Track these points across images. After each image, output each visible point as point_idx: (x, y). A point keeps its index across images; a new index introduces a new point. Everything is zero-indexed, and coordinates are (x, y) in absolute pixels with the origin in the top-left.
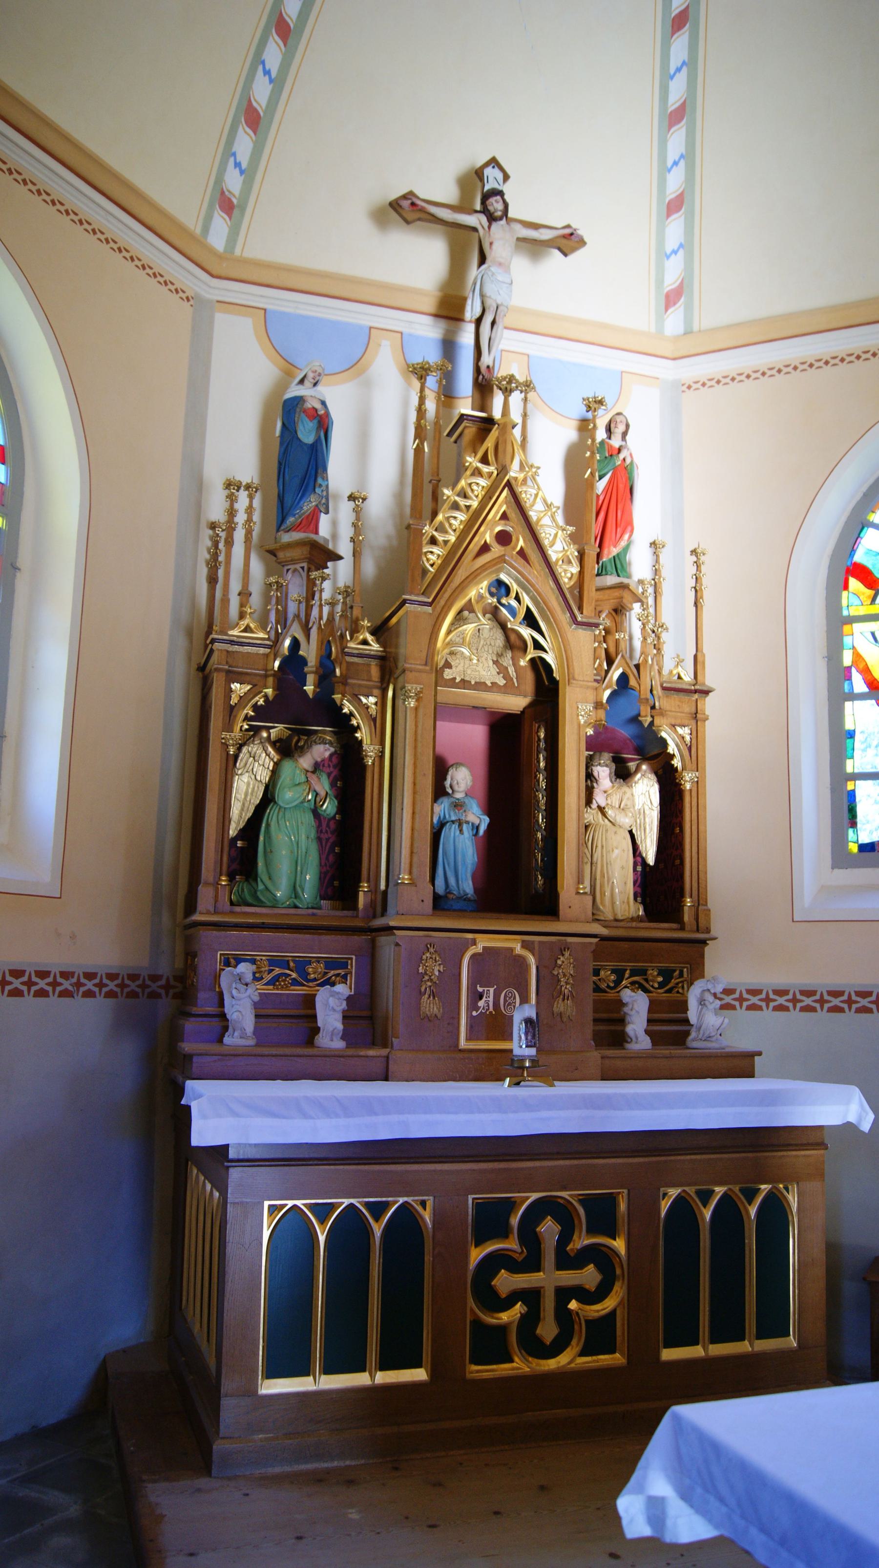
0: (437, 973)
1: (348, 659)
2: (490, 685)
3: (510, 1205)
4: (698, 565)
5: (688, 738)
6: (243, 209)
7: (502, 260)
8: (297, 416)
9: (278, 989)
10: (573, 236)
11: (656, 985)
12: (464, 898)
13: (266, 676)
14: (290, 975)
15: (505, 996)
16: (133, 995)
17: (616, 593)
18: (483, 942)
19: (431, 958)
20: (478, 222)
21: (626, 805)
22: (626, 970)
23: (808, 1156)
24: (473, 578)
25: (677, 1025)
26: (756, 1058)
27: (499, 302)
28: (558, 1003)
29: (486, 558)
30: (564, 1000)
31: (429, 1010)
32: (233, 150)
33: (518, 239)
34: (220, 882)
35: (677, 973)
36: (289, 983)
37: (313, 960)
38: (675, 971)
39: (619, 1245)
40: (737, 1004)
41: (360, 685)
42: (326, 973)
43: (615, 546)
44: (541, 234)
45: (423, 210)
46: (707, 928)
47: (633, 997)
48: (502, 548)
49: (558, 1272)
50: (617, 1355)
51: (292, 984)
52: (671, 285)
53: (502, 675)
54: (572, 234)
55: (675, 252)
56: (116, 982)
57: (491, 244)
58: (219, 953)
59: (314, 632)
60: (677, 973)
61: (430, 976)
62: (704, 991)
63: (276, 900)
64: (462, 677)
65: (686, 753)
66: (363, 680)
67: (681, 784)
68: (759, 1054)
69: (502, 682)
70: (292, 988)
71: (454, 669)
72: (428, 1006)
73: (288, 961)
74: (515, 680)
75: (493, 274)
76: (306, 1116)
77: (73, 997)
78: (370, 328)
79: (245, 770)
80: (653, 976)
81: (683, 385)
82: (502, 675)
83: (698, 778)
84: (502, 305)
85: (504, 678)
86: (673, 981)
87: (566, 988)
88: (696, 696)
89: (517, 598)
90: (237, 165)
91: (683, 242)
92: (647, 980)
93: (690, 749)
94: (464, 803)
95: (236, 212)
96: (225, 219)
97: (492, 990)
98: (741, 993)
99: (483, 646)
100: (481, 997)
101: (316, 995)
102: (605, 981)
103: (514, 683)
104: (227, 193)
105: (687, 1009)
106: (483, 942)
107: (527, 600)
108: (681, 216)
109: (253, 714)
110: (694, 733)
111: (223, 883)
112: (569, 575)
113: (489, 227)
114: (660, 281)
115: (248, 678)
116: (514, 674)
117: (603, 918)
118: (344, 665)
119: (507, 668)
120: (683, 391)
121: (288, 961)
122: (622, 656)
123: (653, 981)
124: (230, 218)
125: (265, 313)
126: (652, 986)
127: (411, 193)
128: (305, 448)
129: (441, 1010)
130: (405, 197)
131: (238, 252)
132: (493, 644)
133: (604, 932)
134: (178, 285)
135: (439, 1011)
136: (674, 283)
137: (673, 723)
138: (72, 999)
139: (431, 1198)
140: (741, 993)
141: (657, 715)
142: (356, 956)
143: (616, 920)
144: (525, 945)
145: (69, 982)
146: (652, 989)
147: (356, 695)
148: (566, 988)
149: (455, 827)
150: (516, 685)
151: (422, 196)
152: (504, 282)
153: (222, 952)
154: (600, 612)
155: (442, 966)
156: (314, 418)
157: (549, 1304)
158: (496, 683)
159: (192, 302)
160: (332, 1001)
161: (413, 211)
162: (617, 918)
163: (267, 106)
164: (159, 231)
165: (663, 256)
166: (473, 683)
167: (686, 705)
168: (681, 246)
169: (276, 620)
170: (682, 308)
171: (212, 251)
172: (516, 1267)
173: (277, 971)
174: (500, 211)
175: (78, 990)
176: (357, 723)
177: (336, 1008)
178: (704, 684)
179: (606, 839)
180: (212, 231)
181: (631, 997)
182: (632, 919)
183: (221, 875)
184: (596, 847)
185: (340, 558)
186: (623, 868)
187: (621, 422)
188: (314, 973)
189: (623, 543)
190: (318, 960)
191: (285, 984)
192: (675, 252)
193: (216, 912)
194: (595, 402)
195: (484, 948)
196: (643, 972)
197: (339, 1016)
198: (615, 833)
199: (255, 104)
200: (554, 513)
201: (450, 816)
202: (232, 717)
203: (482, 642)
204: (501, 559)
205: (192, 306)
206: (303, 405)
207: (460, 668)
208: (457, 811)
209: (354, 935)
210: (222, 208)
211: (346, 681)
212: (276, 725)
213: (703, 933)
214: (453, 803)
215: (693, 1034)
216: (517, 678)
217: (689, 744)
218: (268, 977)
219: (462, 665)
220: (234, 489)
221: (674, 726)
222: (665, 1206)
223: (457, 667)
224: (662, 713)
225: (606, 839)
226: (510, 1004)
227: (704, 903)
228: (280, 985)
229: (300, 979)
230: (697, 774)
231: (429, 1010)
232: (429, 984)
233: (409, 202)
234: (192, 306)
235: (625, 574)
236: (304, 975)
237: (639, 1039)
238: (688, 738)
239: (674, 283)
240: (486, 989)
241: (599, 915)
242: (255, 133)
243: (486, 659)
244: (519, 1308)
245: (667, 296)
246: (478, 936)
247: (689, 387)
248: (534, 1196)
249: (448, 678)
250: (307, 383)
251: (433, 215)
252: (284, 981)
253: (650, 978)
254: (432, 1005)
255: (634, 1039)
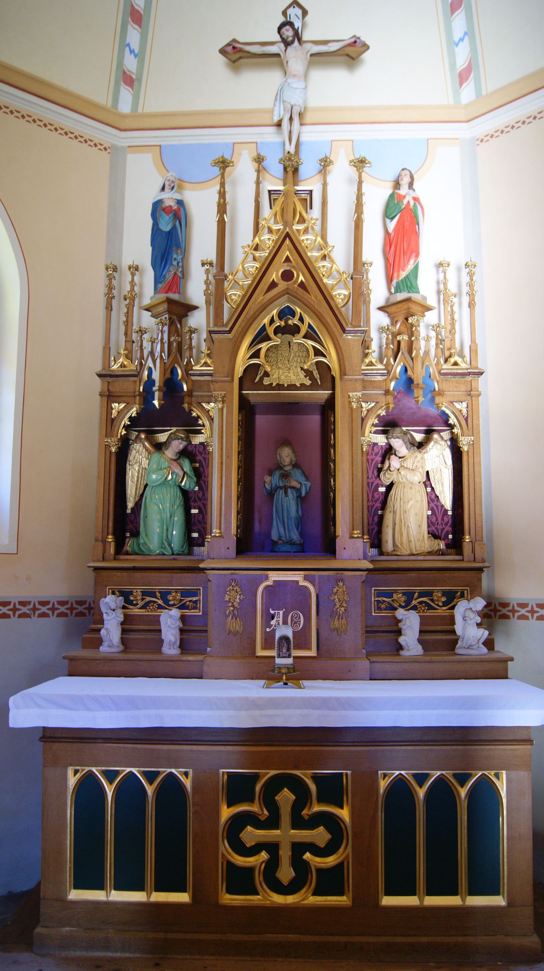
0: (238, 600)
1: (194, 378)
2: (299, 385)
3: (256, 777)
4: (471, 275)
5: (464, 411)
6: (140, 80)
7: (296, 73)
8: (158, 213)
9: (148, 611)
10: (357, 44)
11: (441, 604)
12: (291, 543)
13: (135, 397)
14: (157, 602)
15: (292, 616)
16: (81, 614)
17: (405, 306)
18: (274, 577)
19: (233, 590)
20: (279, 49)
21: (416, 467)
22: (415, 592)
23: (505, 750)
24: (264, 308)
25: (450, 635)
26: (509, 662)
27: (293, 103)
28: (334, 621)
29: (275, 292)
30: (338, 620)
31: (233, 628)
32: (127, 42)
33: (312, 55)
34: (107, 540)
35: (459, 594)
36: (156, 607)
37: (173, 591)
38: (457, 592)
39: (345, 814)
40: (529, 615)
41: (202, 396)
42: (181, 600)
43: (403, 270)
44: (330, 47)
45: (241, 50)
46: (483, 559)
47: (406, 615)
48: (286, 283)
49: (292, 831)
50: (344, 898)
51: (158, 608)
52: (462, 65)
53: (308, 377)
54: (355, 42)
55: (462, 40)
56: (66, 606)
57: (287, 62)
58: (108, 587)
59: (158, 361)
60: (459, 594)
61: (233, 603)
62: (467, 609)
63: (150, 550)
64: (277, 382)
65: (463, 422)
66: (205, 392)
67: (460, 447)
68: (512, 659)
69: (308, 382)
70: (159, 610)
71: (271, 377)
72: (232, 624)
73: (155, 592)
74: (319, 380)
75: (289, 84)
76: (88, 709)
77: (31, 618)
78: (234, 144)
79: (135, 461)
80: (439, 597)
81: (477, 140)
82: (308, 377)
83: (473, 441)
84: (295, 105)
85: (310, 379)
86: (455, 600)
87: (340, 610)
88: (469, 378)
89: (301, 319)
90: (132, 51)
91: (466, 30)
92: (432, 600)
93: (466, 420)
94: (290, 473)
95: (136, 84)
96: (129, 91)
97: (281, 612)
98: (532, 606)
99: (293, 358)
100: (273, 617)
101: (160, 615)
102: (397, 601)
103: (318, 383)
104: (128, 73)
105: (455, 624)
106: (274, 577)
107: (307, 319)
108: (462, 11)
109: (129, 423)
110: (470, 407)
111: (110, 540)
112: (342, 297)
113: (285, 51)
114: (453, 64)
115: (124, 399)
116: (318, 376)
117: (399, 554)
118: (190, 383)
119: (312, 372)
120: (478, 145)
121: (155, 592)
122: (402, 353)
123: (438, 601)
124: (132, 89)
125: (160, 148)
126: (438, 605)
127: (234, 41)
128: (164, 235)
129: (242, 627)
130: (228, 45)
131: (140, 110)
132: (301, 355)
133: (371, 566)
134: (96, 141)
135: (240, 628)
136: (464, 64)
137: (451, 400)
138: (30, 619)
139: (191, 770)
140: (532, 606)
141: (437, 395)
142: (202, 587)
143: (413, 555)
144: (306, 578)
145: (26, 608)
146: (437, 607)
147: (200, 403)
148: (340, 610)
149: (282, 492)
150: (320, 383)
151: (241, 41)
152: (297, 89)
153: (110, 587)
154: (396, 322)
155: (242, 595)
156: (171, 212)
157: (285, 854)
158: (304, 384)
159: (109, 150)
160: (169, 621)
161: (235, 53)
162: (413, 553)
163: (145, 7)
164: (71, 107)
165: (452, 44)
166: (286, 386)
167: (462, 386)
168: (466, 34)
169: (140, 357)
170: (473, 82)
171: (124, 116)
172: (259, 824)
173: (148, 599)
174: (291, 36)
175: (34, 613)
176: (203, 422)
177: (171, 625)
178: (477, 368)
179: (403, 493)
180: (121, 101)
181: (404, 615)
182: (430, 553)
183: (108, 534)
184: (397, 499)
185: (195, 308)
186: (416, 514)
187: (406, 175)
188: (173, 600)
189: (410, 266)
190: (176, 591)
191: (153, 608)
192: (462, 40)
193: (104, 560)
194: (358, 161)
195: (275, 581)
196: (429, 594)
197: (177, 633)
198: (411, 488)
199: (136, 7)
200: (330, 252)
201: (279, 484)
202: (113, 427)
203: (292, 354)
204: (287, 292)
205: (109, 153)
206: (162, 205)
207: (276, 376)
208: (284, 480)
209: (200, 573)
210: (126, 83)
211: (192, 393)
212: (172, 428)
213: (479, 562)
214: (282, 474)
215: (460, 643)
216: (320, 379)
217: (466, 416)
218: (141, 603)
219: (277, 373)
220: (111, 271)
221: (452, 402)
222: (383, 784)
223: (273, 375)
224: (441, 393)
225: (403, 493)
226: (296, 623)
227: (480, 539)
228: (150, 609)
229: (163, 604)
230: (472, 438)
231: (233, 628)
232: (232, 608)
233: (231, 47)
234: (109, 153)
235: (414, 290)
236: (166, 601)
237: (410, 648)
238: (464, 411)
239: (464, 64)
240: (277, 612)
241: (398, 551)
242: (140, 27)
243: (296, 367)
244: (264, 855)
245: (460, 75)
246: (270, 573)
247: (482, 141)
248: (273, 772)
249: (266, 384)
250: (166, 189)
251: (248, 52)
252: (153, 606)
253: (435, 598)
254: (234, 624)
255: (407, 648)
